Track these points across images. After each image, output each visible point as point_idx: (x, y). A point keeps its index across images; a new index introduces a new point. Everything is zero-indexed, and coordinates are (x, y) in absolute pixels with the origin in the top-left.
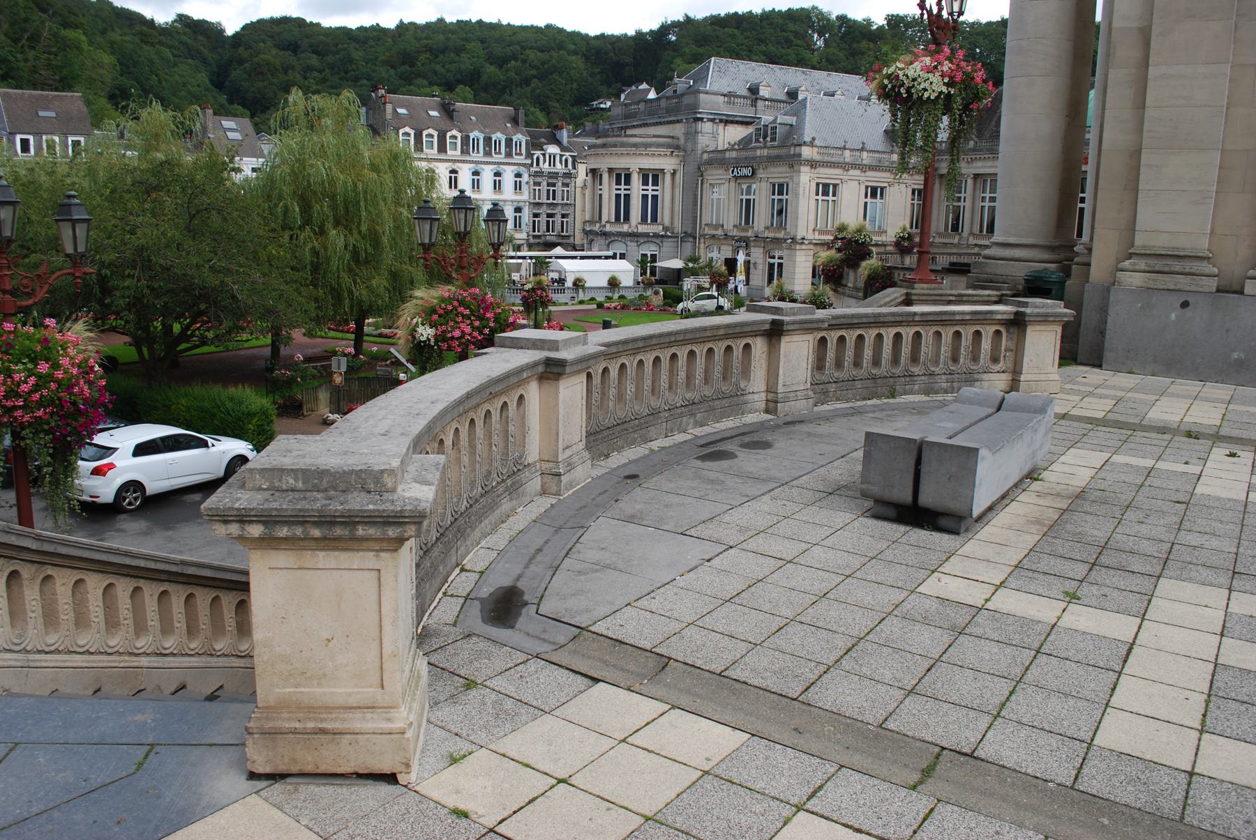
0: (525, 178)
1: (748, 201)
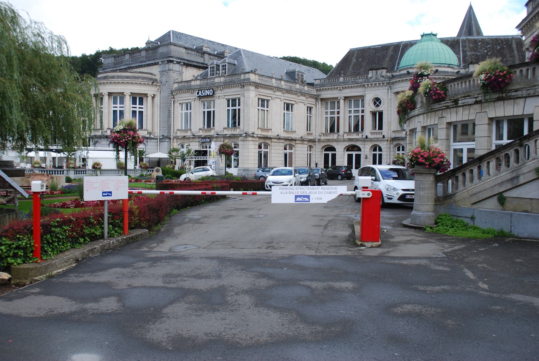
1: (209, 113)
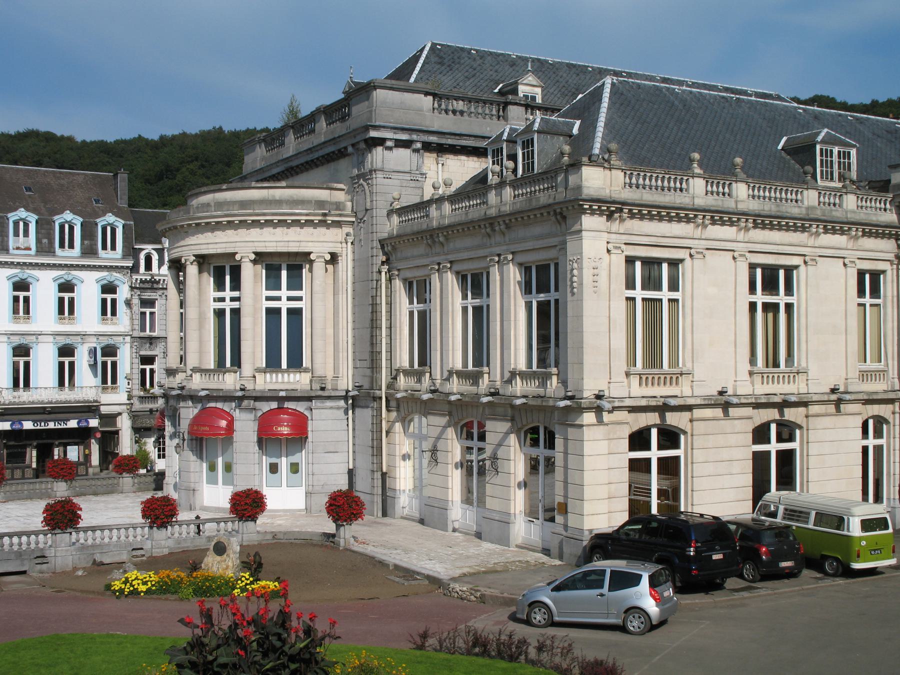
0: (123, 292)
